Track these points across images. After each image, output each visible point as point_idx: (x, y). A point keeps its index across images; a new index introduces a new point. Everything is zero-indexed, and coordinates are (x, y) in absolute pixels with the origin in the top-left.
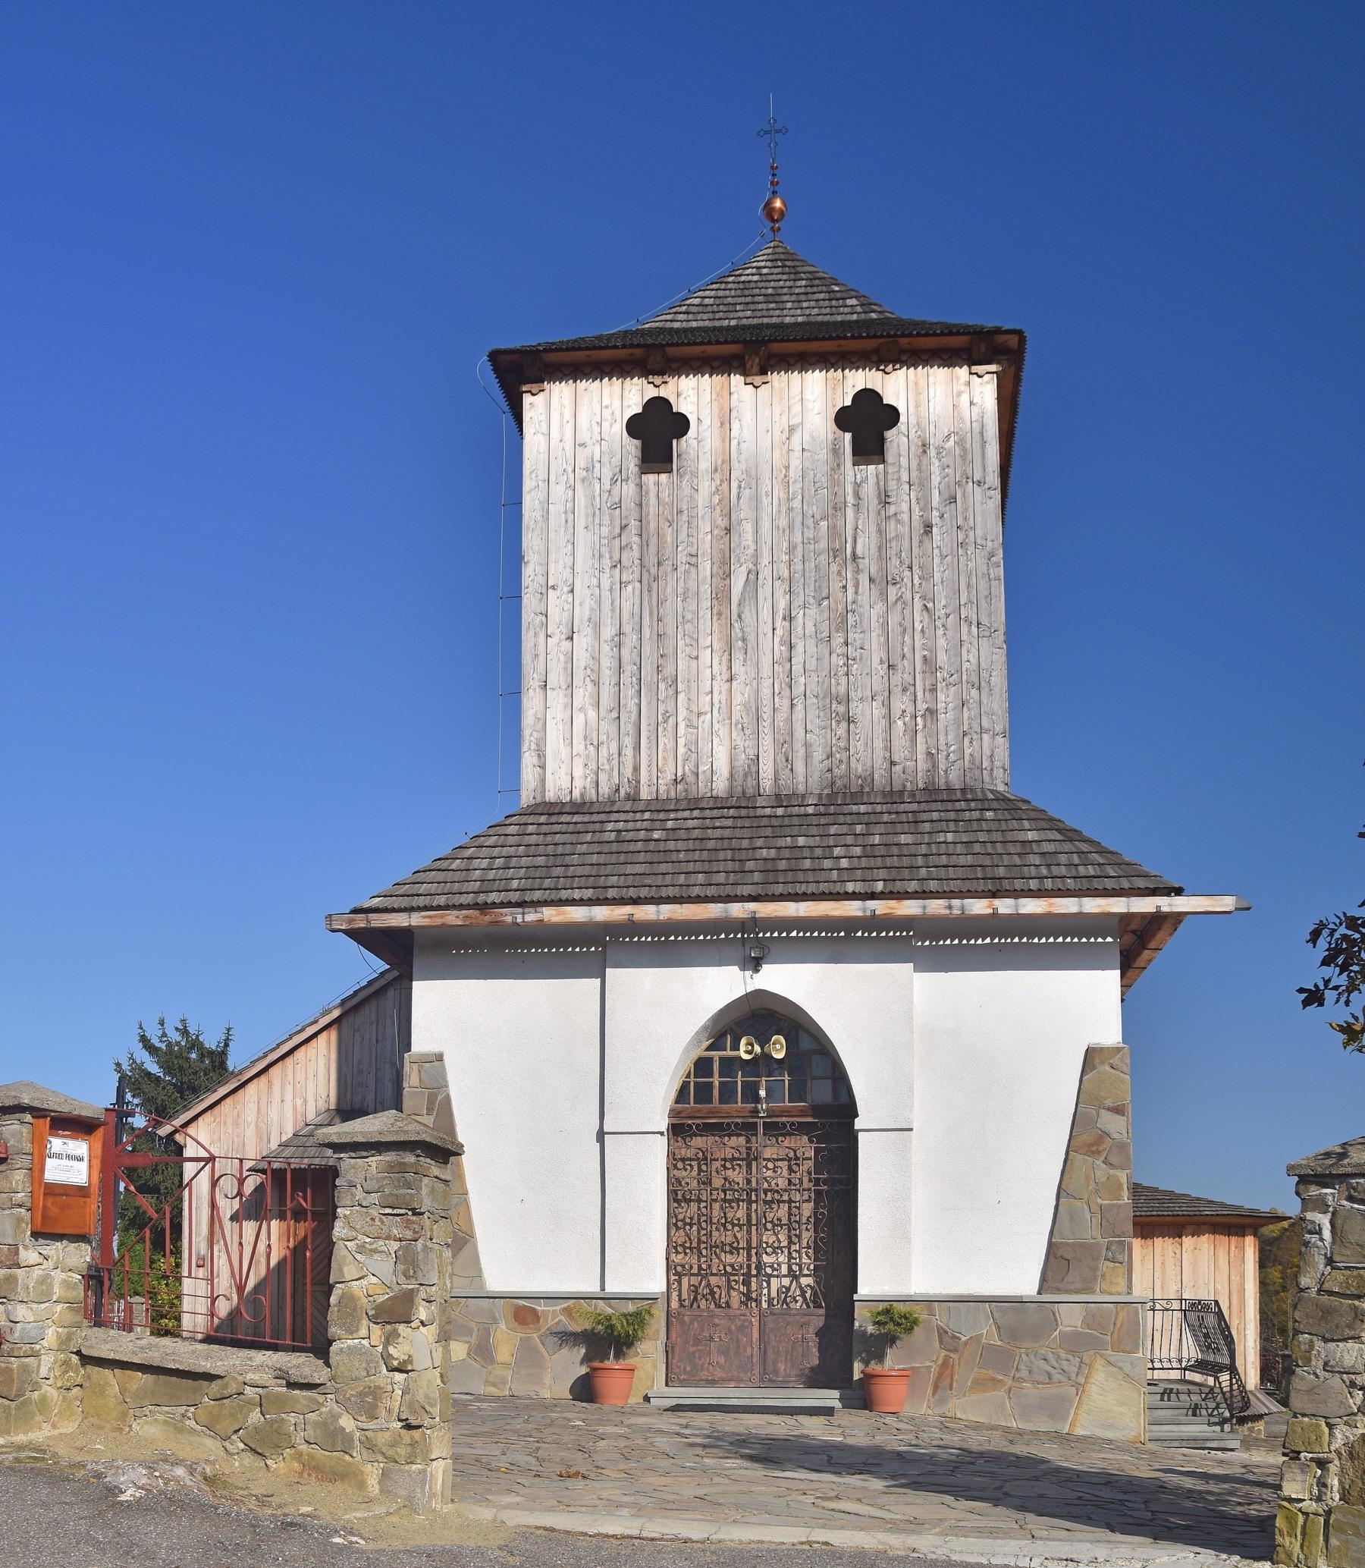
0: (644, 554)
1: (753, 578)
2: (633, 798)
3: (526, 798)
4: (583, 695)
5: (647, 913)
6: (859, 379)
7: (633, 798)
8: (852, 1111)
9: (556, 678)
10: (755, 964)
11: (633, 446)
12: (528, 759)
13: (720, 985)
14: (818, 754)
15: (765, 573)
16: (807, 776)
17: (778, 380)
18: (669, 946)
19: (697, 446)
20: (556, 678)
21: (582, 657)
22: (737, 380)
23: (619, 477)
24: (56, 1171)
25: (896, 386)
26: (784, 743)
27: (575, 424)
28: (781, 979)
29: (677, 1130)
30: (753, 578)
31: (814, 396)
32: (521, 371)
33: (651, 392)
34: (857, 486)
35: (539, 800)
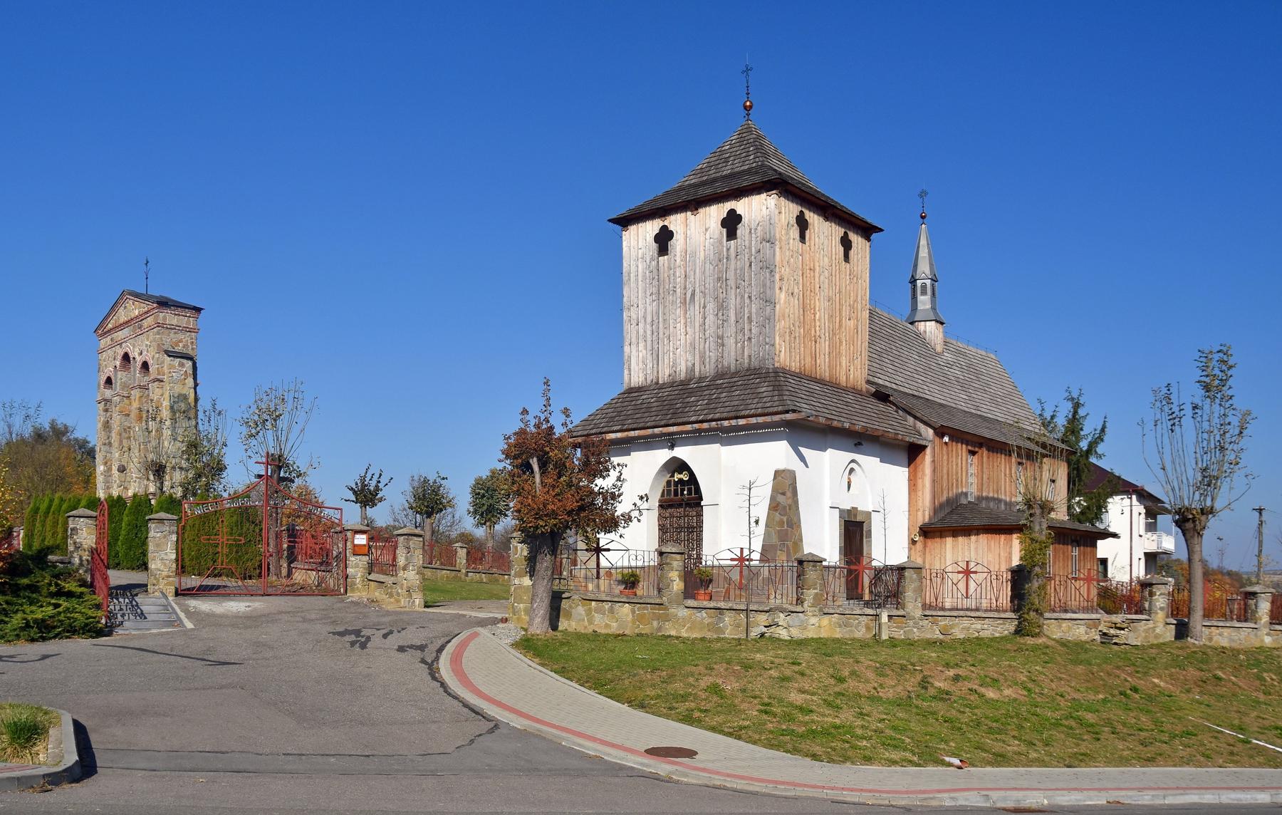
0: (659, 288)
1: (693, 294)
2: (657, 383)
3: (625, 387)
4: (641, 345)
5: (632, 434)
6: (729, 205)
7: (657, 383)
8: (701, 499)
9: (634, 340)
10: (672, 447)
11: (655, 246)
12: (626, 372)
13: (663, 455)
14: (713, 361)
15: (697, 291)
16: (709, 370)
17: (702, 211)
18: (648, 443)
19: (677, 244)
20: (634, 340)
21: (641, 332)
22: (689, 213)
23: (652, 259)
24: (356, 542)
25: (741, 206)
26: (702, 358)
27: (641, 236)
28: (682, 452)
29: (663, 506)
30: (693, 294)
31: (714, 214)
32: (625, 221)
33: (661, 224)
34: (728, 250)
35: (734, 354)
